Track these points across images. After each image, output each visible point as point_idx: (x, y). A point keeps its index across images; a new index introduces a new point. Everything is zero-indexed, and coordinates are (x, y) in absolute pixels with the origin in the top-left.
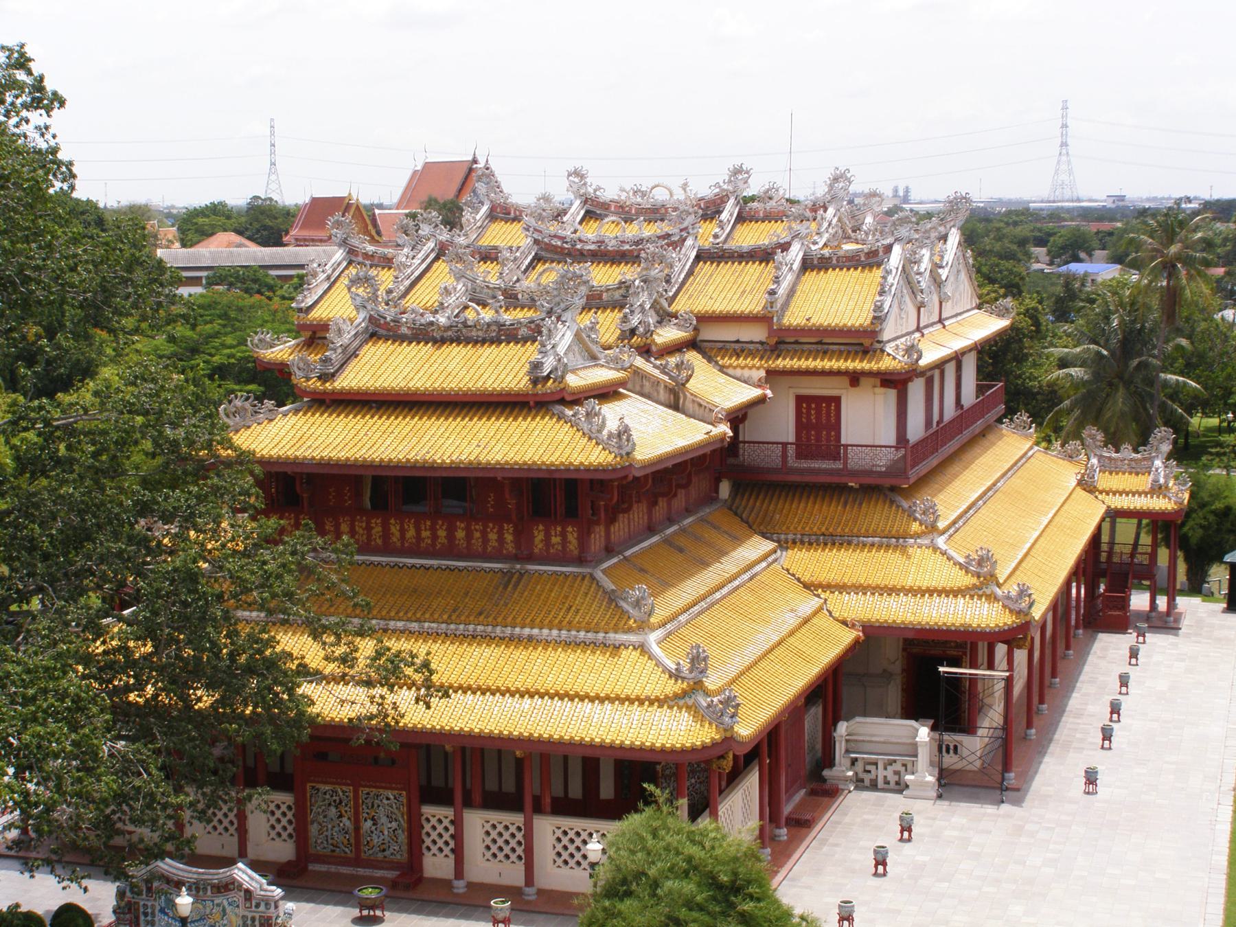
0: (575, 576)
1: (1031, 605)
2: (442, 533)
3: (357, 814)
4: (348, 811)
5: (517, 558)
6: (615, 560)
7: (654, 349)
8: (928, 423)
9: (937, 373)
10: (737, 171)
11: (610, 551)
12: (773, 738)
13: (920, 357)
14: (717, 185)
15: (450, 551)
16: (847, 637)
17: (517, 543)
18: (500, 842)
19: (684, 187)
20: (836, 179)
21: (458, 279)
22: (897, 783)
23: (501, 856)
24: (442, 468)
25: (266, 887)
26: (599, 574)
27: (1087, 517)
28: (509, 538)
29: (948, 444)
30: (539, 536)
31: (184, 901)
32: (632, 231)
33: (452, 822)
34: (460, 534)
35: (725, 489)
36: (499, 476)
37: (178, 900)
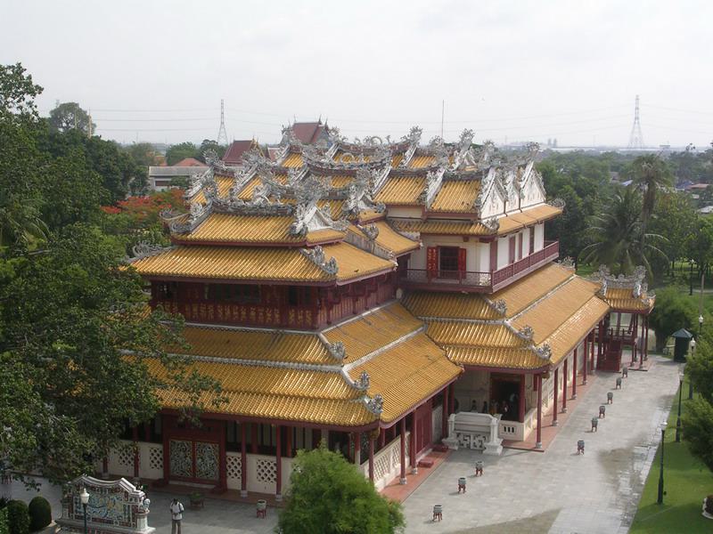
0: (309, 335)
1: (550, 356)
2: (244, 313)
3: (194, 456)
4: (189, 454)
5: (280, 326)
6: (332, 328)
7: (360, 221)
8: (512, 260)
9: (517, 235)
10: (415, 130)
11: (329, 323)
12: (407, 422)
13: (498, 228)
14: (405, 137)
15: (248, 323)
16: (456, 370)
17: (281, 319)
18: (266, 471)
19: (388, 137)
20: (465, 135)
21: (264, 184)
22: (481, 446)
23: (266, 478)
24: (242, 279)
25: (135, 490)
26: (321, 335)
27: (596, 309)
28: (277, 316)
29: (523, 270)
30: (292, 316)
31: (86, 495)
32: (353, 161)
33: (275, 464)
34: (253, 314)
35: (399, 293)
36: (270, 284)
37: (83, 495)
